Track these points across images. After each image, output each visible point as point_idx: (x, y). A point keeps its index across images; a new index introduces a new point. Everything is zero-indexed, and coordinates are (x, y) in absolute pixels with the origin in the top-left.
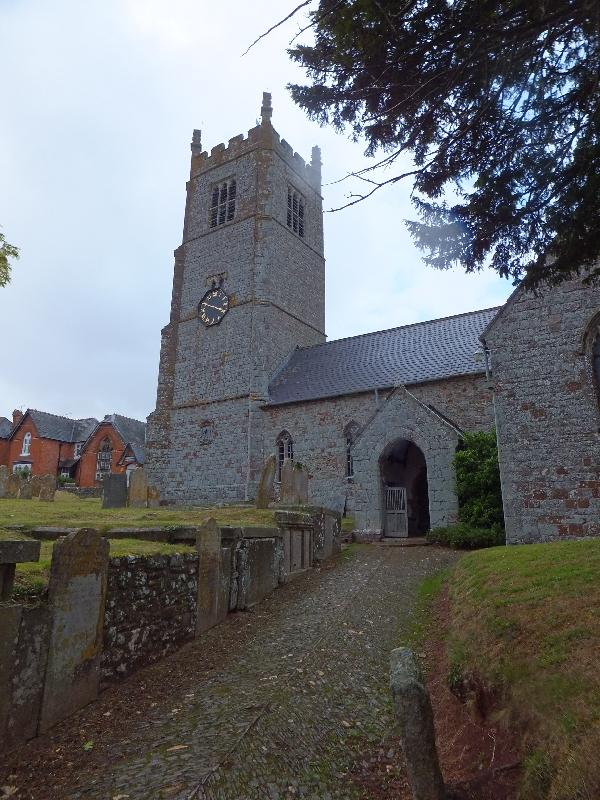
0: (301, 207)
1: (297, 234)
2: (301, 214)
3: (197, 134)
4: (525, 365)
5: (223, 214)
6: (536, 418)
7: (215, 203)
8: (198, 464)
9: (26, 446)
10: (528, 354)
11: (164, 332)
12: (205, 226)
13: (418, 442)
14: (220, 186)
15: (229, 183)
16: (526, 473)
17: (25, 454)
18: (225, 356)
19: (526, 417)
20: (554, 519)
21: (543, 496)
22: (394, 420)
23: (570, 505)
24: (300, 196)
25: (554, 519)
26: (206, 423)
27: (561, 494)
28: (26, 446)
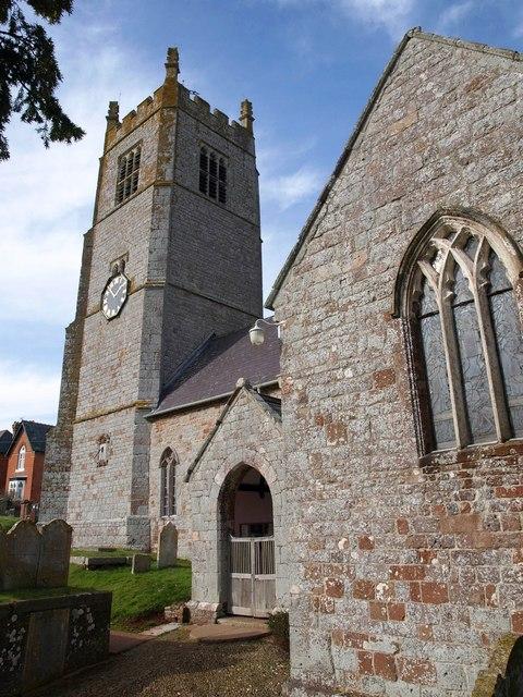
0: (223, 170)
1: (208, 197)
2: (223, 176)
3: (114, 107)
4: (320, 345)
5: (129, 188)
6: (331, 441)
7: (123, 177)
8: (95, 492)
9: (22, 460)
10: (325, 325)
11: (68, 330)
12: (113, 203)
13: (264, 470)
14: (127, 156)
15: (135, 151)
16: (317, 545)
17: (21, 469)
18: (122, 354)
19: (319, 440)
20: (355, 639)
21: (337, 590)
22: (236, 436)
23: (376, 614)
24: (219, 156)
25: (355, 639)
26: (102, 439)
27: (365, 590)
28: (22, 460)
